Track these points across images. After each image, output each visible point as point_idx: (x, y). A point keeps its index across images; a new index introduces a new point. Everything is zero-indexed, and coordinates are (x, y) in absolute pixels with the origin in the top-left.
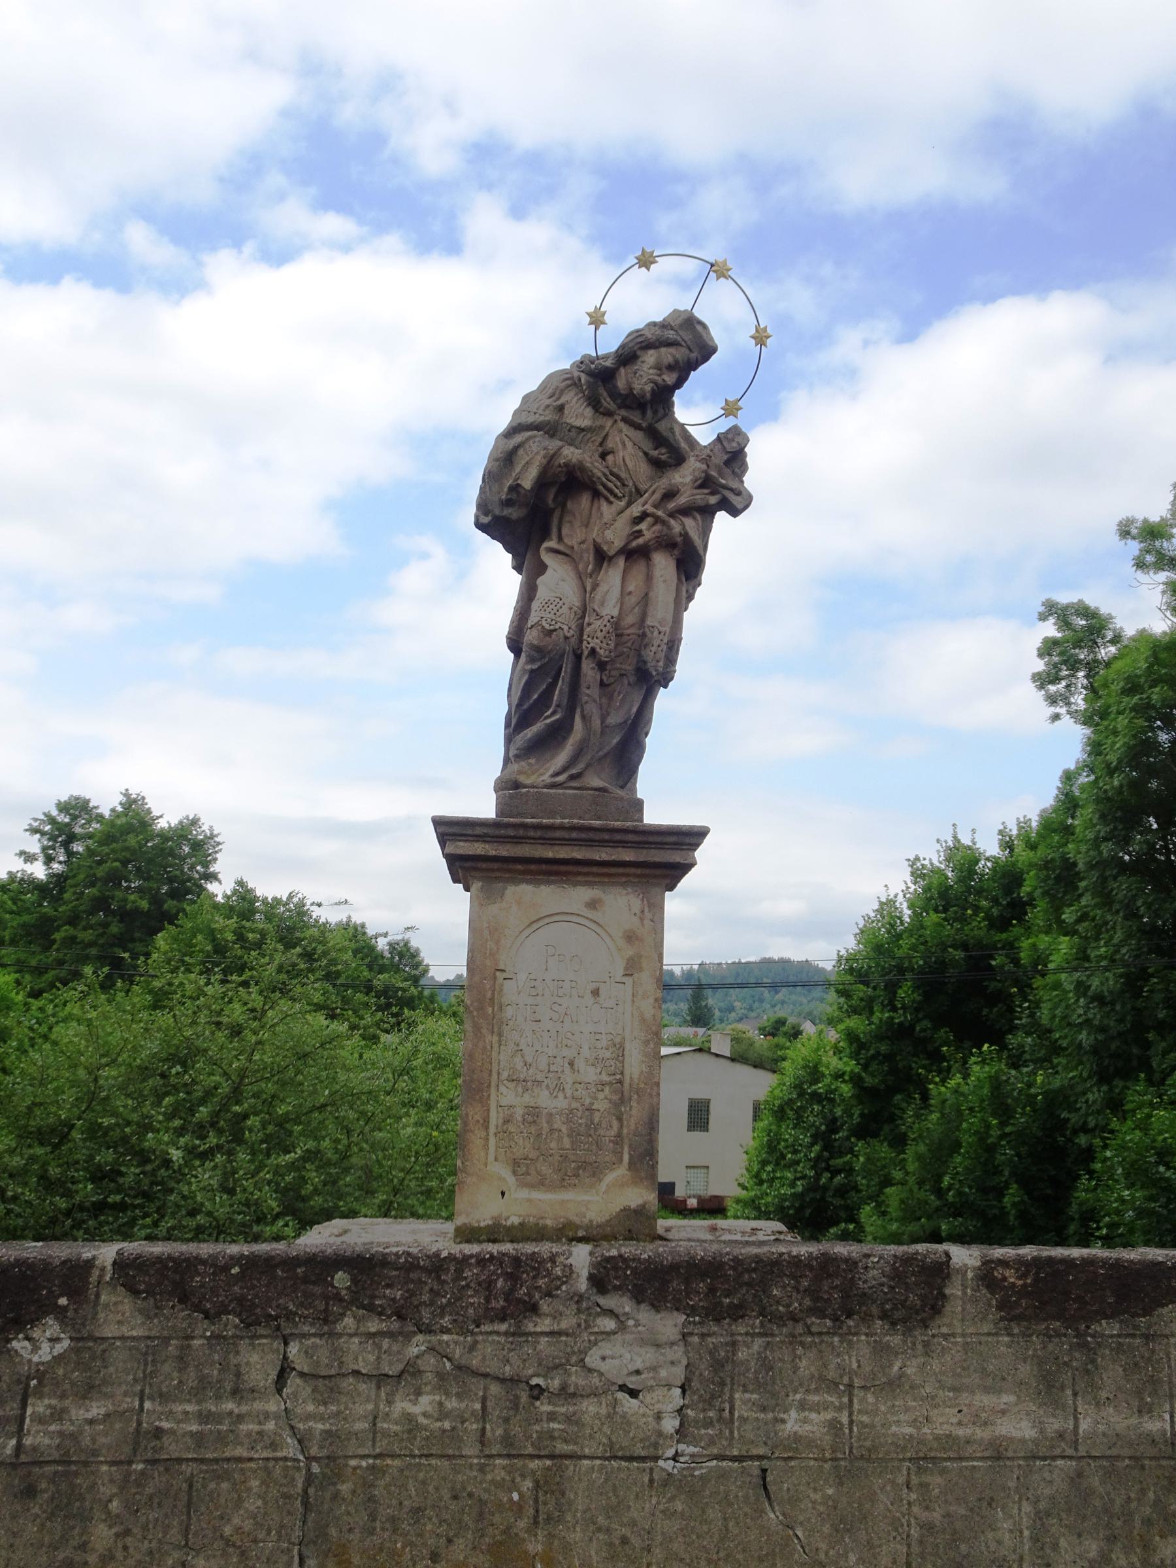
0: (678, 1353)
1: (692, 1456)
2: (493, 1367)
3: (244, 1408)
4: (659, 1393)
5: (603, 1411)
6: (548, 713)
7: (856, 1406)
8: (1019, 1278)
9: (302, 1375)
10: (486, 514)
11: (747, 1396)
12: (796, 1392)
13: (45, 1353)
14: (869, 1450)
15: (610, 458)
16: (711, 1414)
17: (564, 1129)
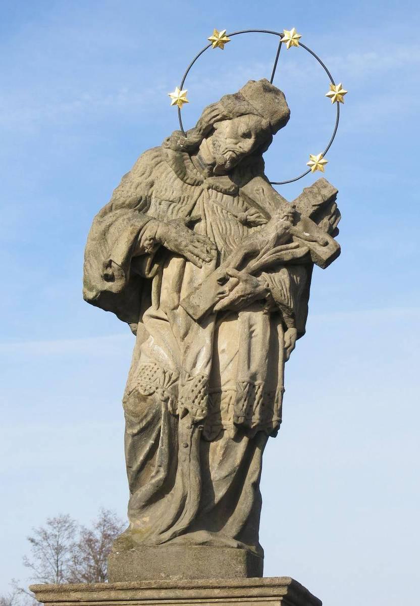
6: (153, 474)
10: (91, 289)
15: (199, 227)
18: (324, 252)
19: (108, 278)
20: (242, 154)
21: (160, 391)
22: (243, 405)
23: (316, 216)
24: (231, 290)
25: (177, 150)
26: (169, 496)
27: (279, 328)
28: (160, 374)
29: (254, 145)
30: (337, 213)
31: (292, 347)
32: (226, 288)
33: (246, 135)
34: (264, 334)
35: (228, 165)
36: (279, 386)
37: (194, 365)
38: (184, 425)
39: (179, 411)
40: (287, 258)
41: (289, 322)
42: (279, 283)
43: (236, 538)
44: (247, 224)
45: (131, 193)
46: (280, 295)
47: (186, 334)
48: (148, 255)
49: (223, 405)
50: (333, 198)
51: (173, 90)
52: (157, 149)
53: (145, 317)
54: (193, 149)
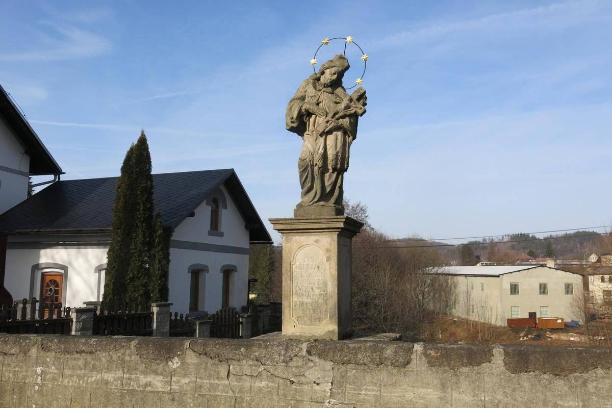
0: (331, 374)
1: (334, 402)
2: (281, 375)
3: (220, 383)
4: (325, 384)
5: (310, 389)
7: (382, 391)
8: (436, 354)
9: (233, 374)
11: (350, 386)
12: (364, 386)
13: (175, 366)
14: (386, 403)
15: (321, 104)
16: (340, 391)
17: (311, 308)
18: (360, 111)
19: (293, 122)
20: (334, 80)
21: (308, 158)
22: (161, 197)
23: (358, 100)
24: (330, 125)
25: (313, 79)
26: (312, 191)
27: (347, 137)
28: (308, 152)
29: (337, 76)
30: (366, 98)
31: (351, 143)
32: (328, 124)
33: (335, 74)
34: (341, 138)
35: (329, 84)
36: (347, 155)
37: (319, 149)
38: (316, 169)
39: (314, 165)
40: (348, 114)
41: (350, 134)
42: (346, 122)
43: (334, 204)
44: (337, 103)
45: (300, 95)
46: (348, 126)
47: (316, 139)
48: (304, 115)
49: (329, 162)
50: (365, 93)
51: (312, 60)
52: (308, 79)
53: (305, 135)
54: (318, 79)
